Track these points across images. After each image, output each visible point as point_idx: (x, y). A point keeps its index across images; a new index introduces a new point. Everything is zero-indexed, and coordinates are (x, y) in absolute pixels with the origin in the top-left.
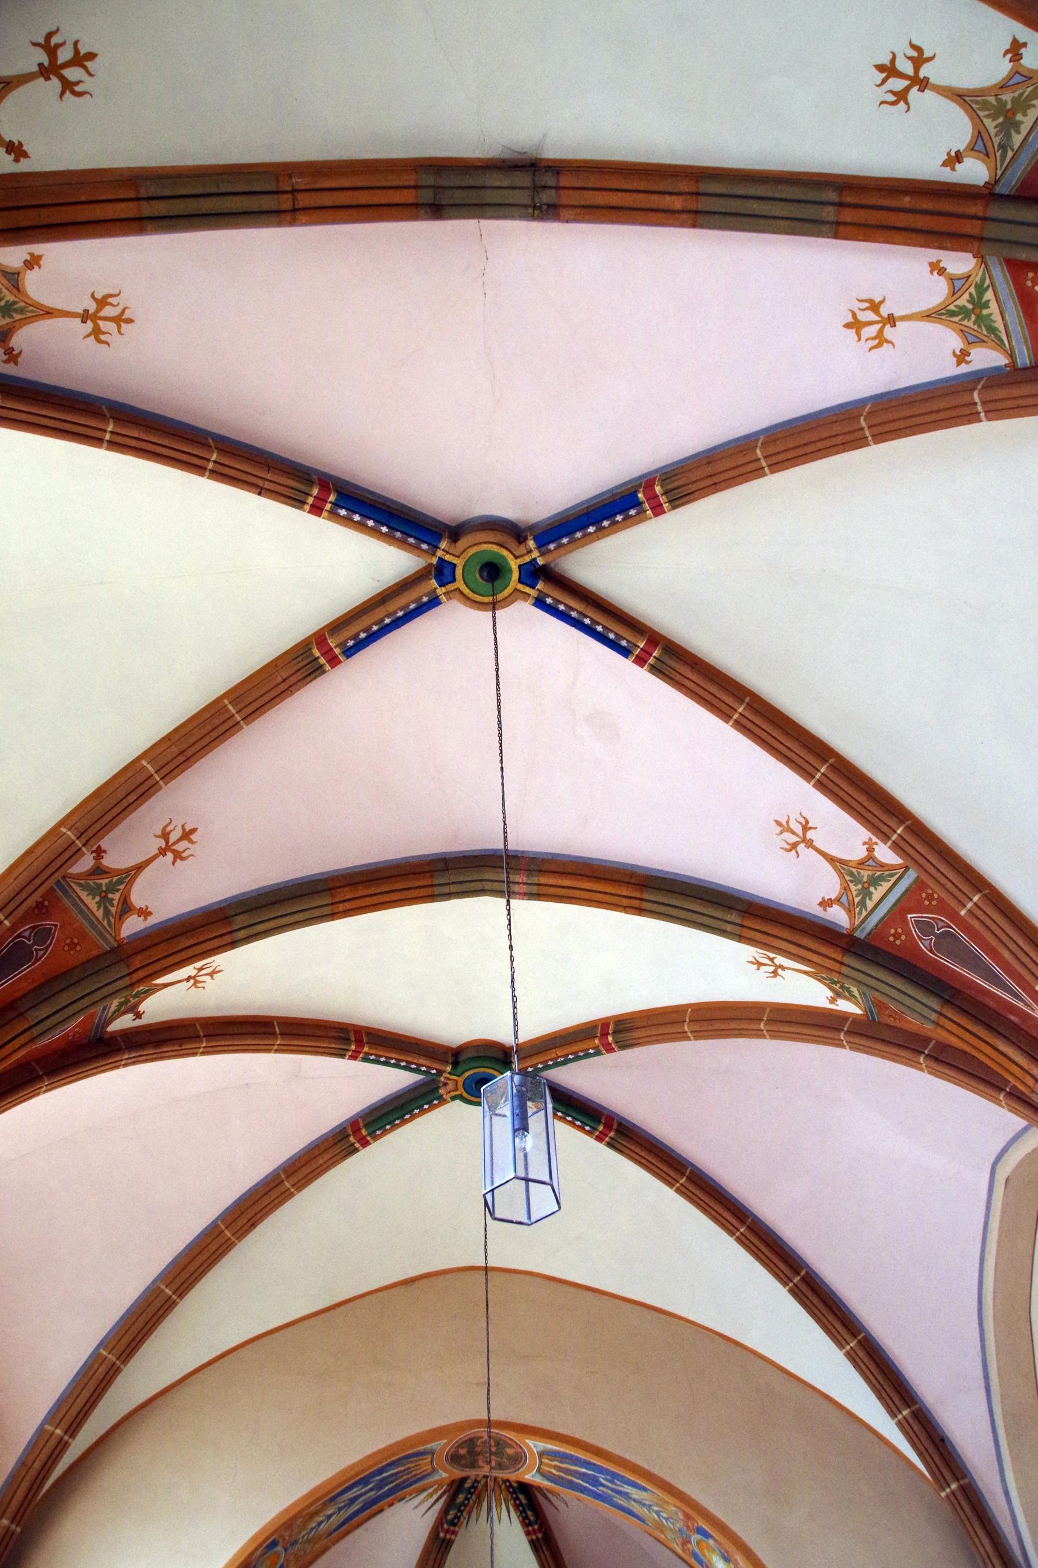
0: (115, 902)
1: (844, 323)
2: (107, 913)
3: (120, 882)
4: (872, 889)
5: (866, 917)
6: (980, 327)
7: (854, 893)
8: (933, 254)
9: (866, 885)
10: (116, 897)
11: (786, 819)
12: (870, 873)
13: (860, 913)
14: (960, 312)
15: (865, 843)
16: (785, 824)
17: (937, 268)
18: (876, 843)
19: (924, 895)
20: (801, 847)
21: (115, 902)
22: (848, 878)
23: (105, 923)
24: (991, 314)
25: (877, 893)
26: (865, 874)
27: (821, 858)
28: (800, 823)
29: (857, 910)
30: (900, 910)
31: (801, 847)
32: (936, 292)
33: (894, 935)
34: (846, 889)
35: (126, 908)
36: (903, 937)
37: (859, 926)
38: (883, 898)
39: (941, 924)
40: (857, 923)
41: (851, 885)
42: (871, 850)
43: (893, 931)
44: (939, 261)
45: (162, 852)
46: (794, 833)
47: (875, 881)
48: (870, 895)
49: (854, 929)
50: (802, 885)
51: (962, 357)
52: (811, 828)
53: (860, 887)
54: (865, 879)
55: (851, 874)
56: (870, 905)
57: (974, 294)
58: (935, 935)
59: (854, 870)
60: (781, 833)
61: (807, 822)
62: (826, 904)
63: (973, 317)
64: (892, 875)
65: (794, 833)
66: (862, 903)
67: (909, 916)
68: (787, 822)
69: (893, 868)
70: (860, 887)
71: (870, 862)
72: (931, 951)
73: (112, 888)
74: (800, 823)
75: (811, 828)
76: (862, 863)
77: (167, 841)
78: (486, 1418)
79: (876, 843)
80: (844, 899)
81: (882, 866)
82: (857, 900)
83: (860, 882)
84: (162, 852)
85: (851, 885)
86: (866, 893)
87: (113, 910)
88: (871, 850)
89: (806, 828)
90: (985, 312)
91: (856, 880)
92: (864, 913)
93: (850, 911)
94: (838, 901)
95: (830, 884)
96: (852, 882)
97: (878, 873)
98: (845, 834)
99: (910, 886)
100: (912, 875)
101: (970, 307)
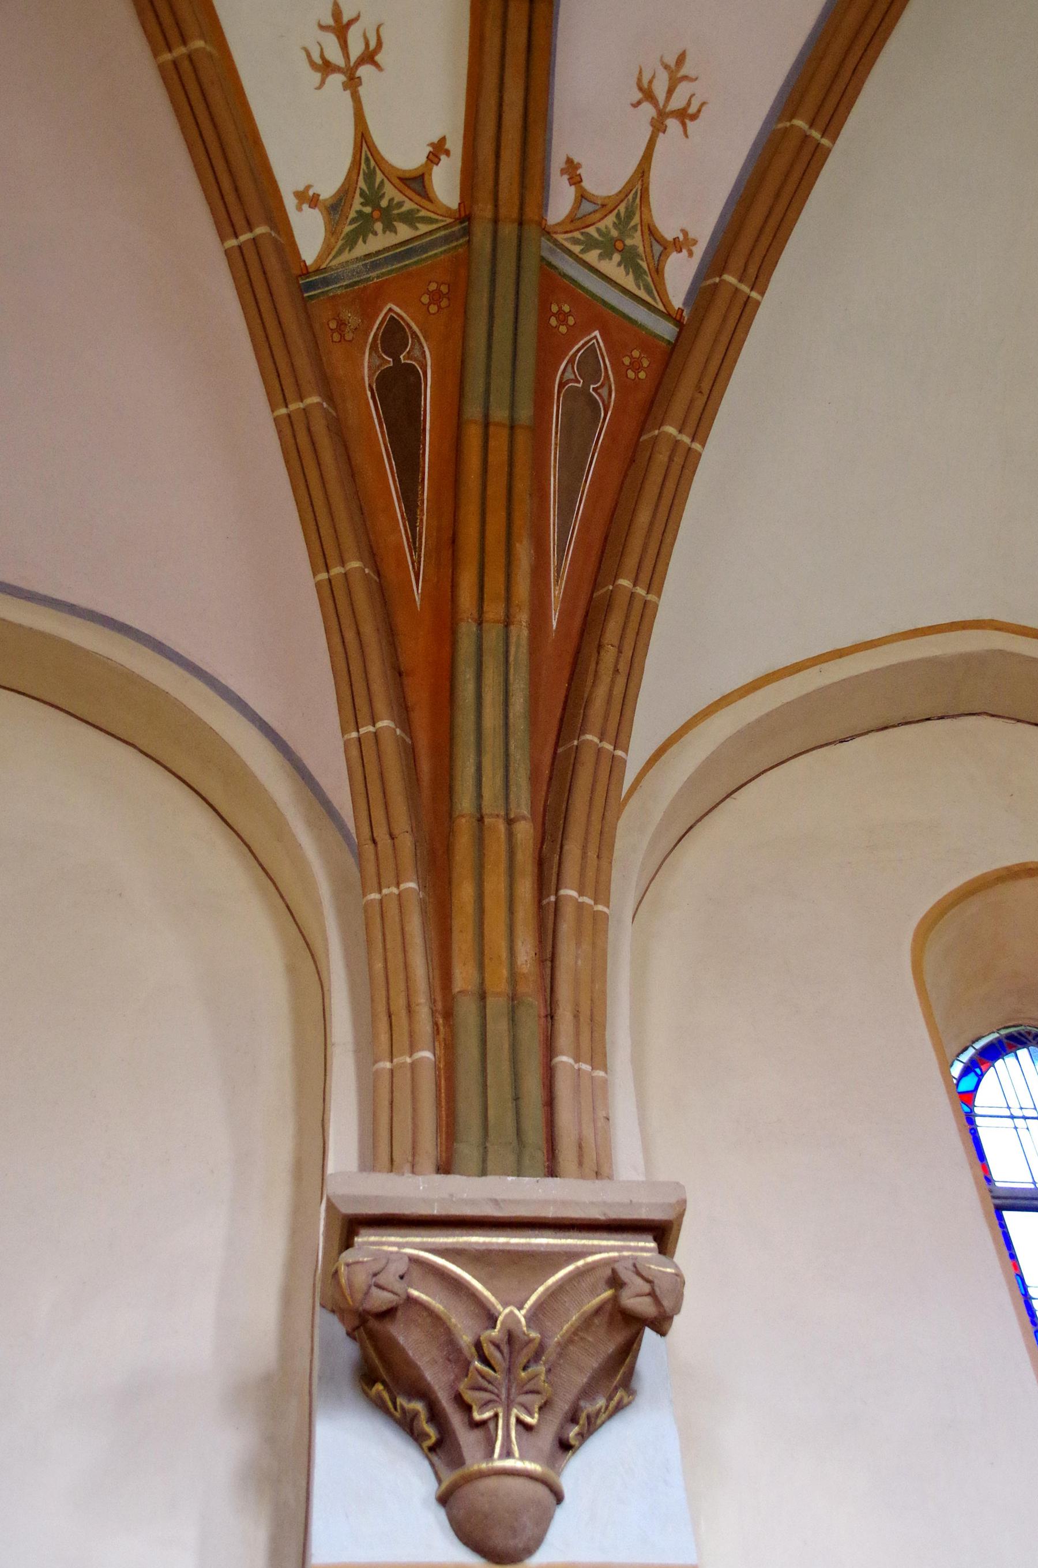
0: (398, 197)
1: (687, 53)
2: (409, 218)
3: (370, 177)
4: (617, 257)
5: (570, 253)
6: (353, 221)
7: (601, 225)
8: (456, 145)
9: (619, 245)
10: (390, 192)
11: (692, 74)
12: (641, 249)
13: (576, 241)
14: (371, 189)
15: (685, 233)
16: (683, 72)
17: (437, 151)
18: (691, 254)
19: (636, 354)
20: (337, 79)
21: (398, 197)
22: (622, 208)
23: (423, 228)
24: (376, 234)
25: (611, 267)
26: (636, 240)
27: (640, 153)
28: (689, 104)
29: (577, 235)
30: (597, 314)
31: (337, 79)
32: (404, 154)
33: (560, 311)
34: (605, 207)
35: (416, 183)
36: (563, 329)
37: (556, 243)
38: (606, 279)
39: (604, 392)
40: (560, 238)
41: (611, 219)
42: (677, 245)
43: (566, 308)
44: (447, 153)
45: (658, 126)
46: (670, 92)
47: (630, 260)
48: (606, 255)
49: (547, 232)
50: (594, 133)
51: (307, 198)
52: (684, 125)
53: (614, 233)
54: (629, 242)
55: (630, 215)
56: (592, 257)
57: (404, 209)
58: (586, 386)
59: (636, 219)
60: (666, 67)
61: (694, 117)
62: (572, 170)
63: (368, 210)
64: (649, 292)
65: (670, 92)
66: (590, 244)
67: (597, 333)
68: (685, 78)
69: (659, 287)
70: (614, 233)
71: (657, 249)
72: (562, 385)
73: (372, 198)
74: (689, 104)
75: (684, 125)
76: (651, 232)
77: (336, 69)
78: (1018, 1052)
79: (691, 254)
80: (587, 207)
81: (658, 271)
82: (592, 231)
83: (622, 233)
84: (658, 126)
85: (611, 219)
86: (609, 247)
87: (408, 206)
88: (677, 245)
89: (684, 116)
90: (378, 226)
91: (622, 223)
92: (577, 249)
93: (575, 221)
94: (583, 196)
95: (606, 178)
96: (618, 215)
97: (644, 265)
98: (692, 198)
99: (642, 327)
100: (666, 330)
101: (384, 203)
